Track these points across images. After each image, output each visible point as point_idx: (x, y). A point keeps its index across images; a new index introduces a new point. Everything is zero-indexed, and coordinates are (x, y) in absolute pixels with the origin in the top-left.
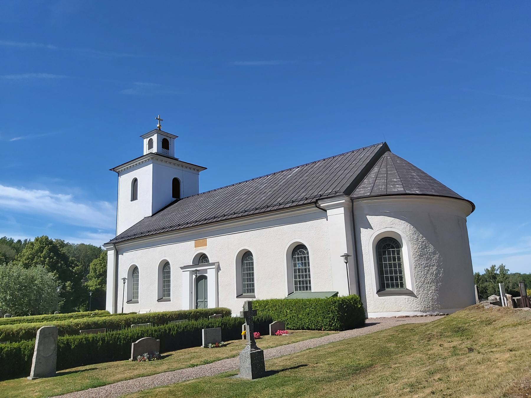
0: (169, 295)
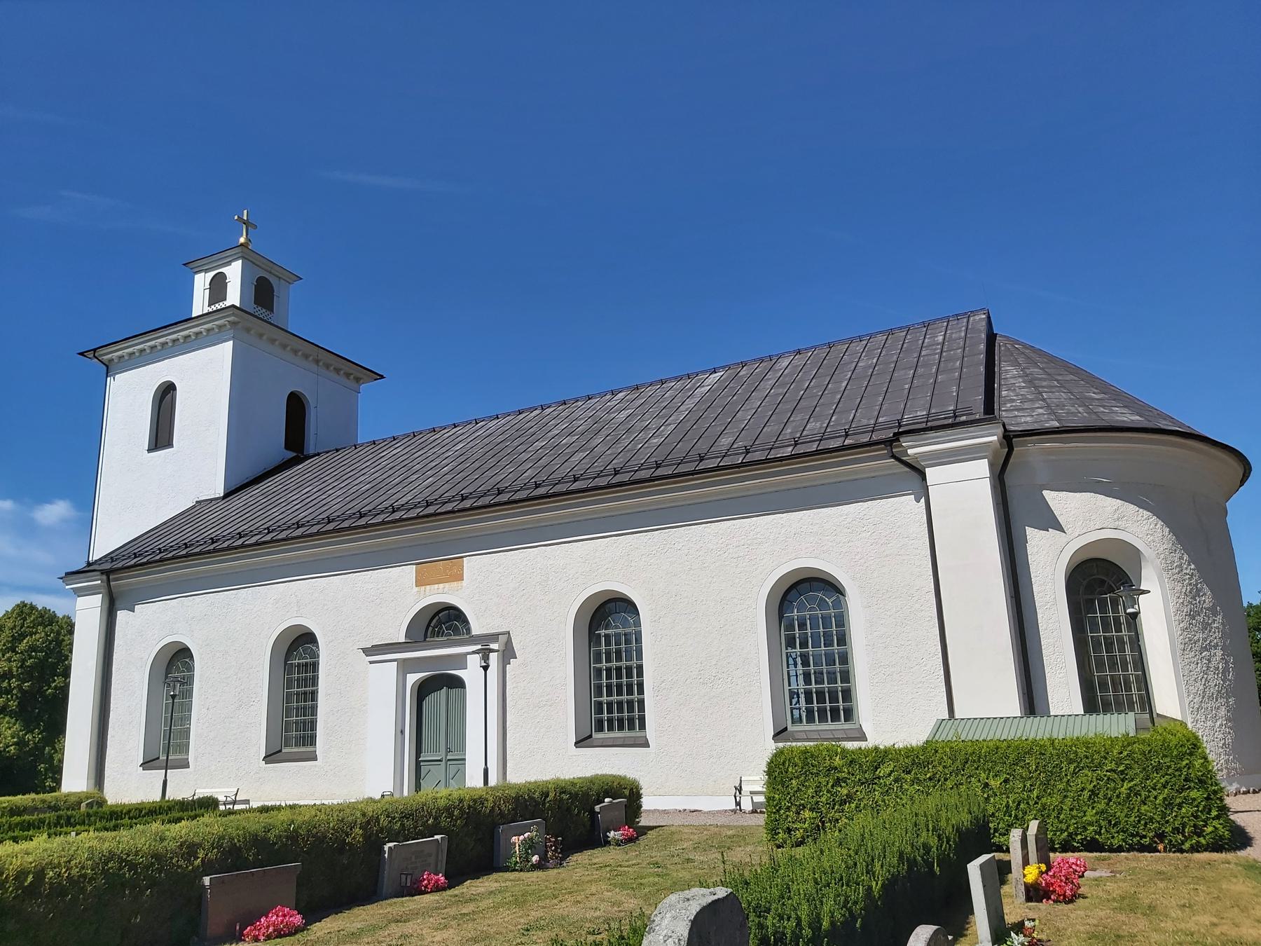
0: (312, 740)
